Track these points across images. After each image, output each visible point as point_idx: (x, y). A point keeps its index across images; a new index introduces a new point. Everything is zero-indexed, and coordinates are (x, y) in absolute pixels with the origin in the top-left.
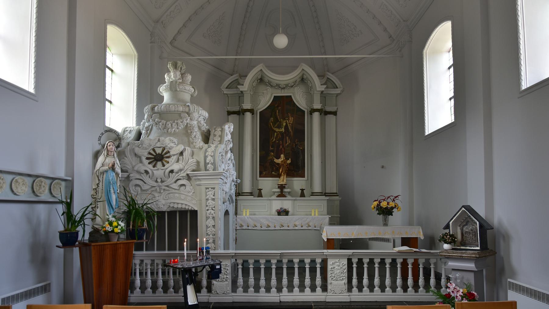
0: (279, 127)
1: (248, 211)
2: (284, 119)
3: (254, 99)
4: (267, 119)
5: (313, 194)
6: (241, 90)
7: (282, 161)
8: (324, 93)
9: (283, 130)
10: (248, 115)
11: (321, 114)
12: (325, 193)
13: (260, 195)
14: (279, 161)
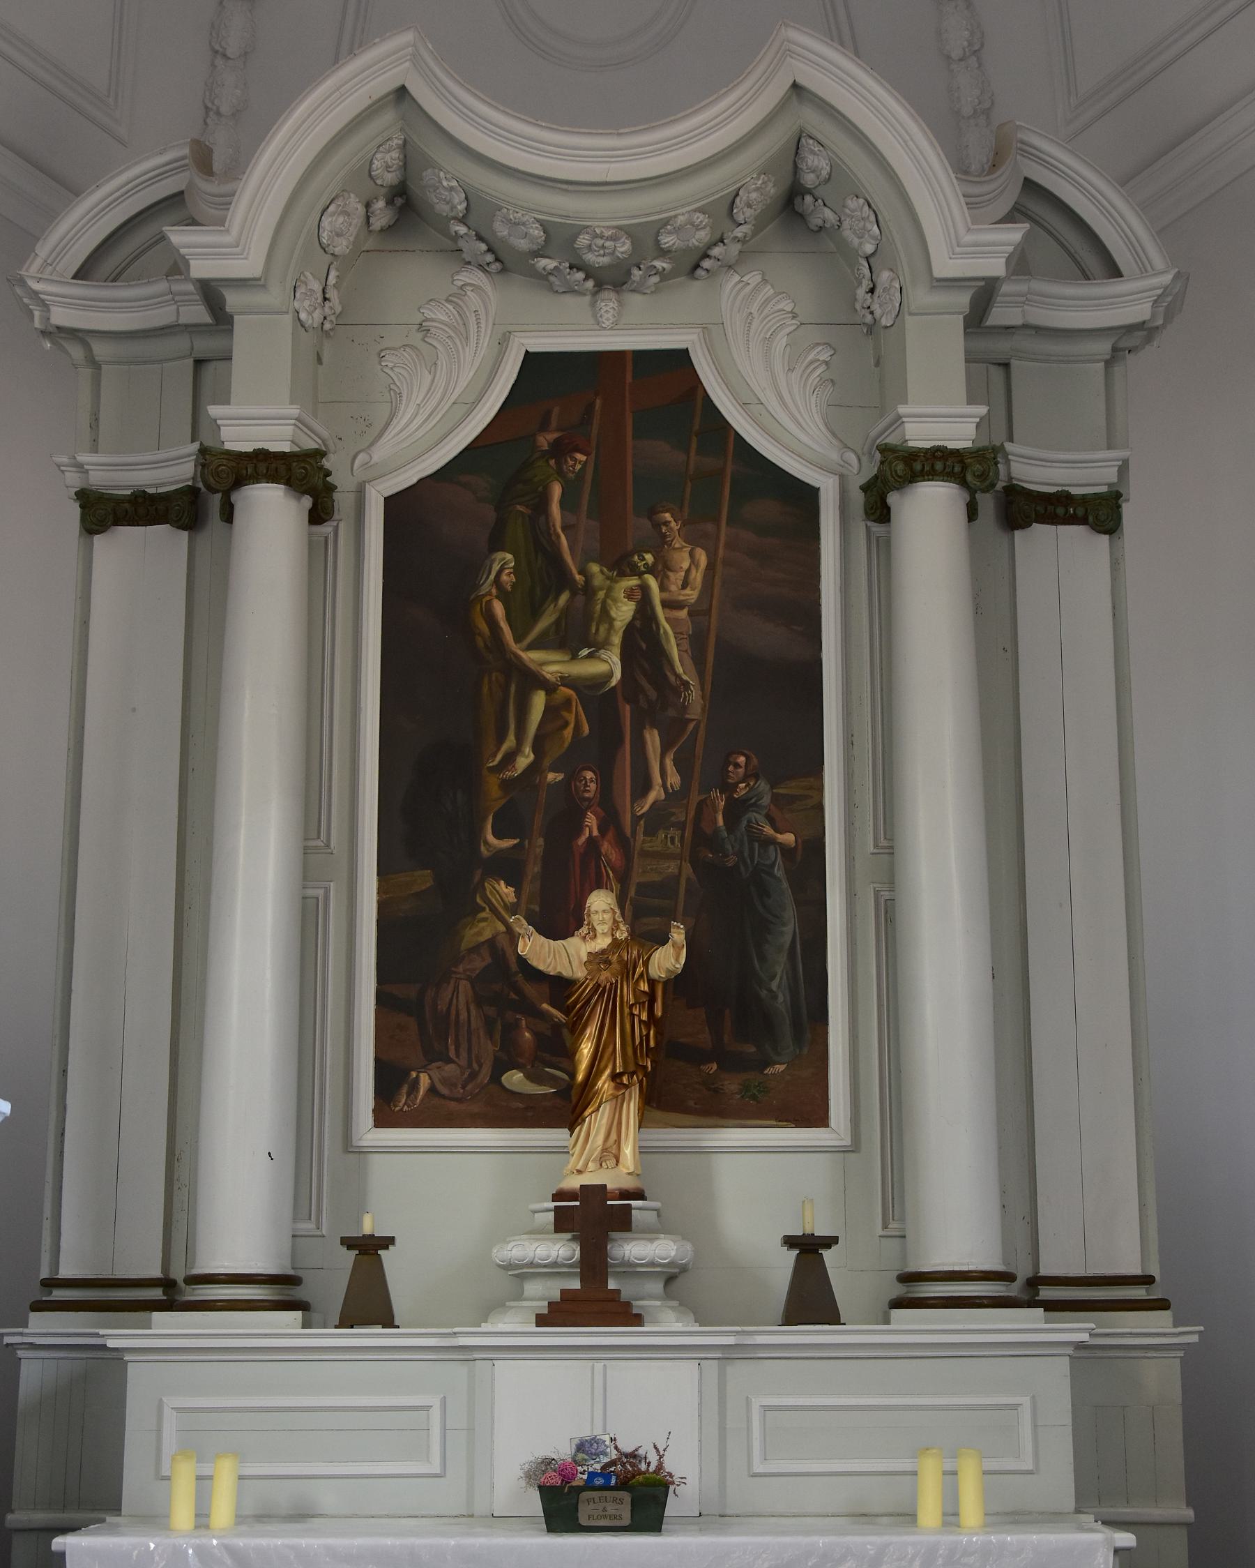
0: (575, 635)
1: (225, 1475)
2: (621, 565)
3: (335, 346)
4: (458, 572)
5: (914, 1290)
6: (201, 268)
7: (598, 960)
8: (999, 315)
9: (610, 664)
10: (270, 511)
11: (972, 512)
12: (1036, 1282)
13: (368, 1305)
14: (566, 957)
